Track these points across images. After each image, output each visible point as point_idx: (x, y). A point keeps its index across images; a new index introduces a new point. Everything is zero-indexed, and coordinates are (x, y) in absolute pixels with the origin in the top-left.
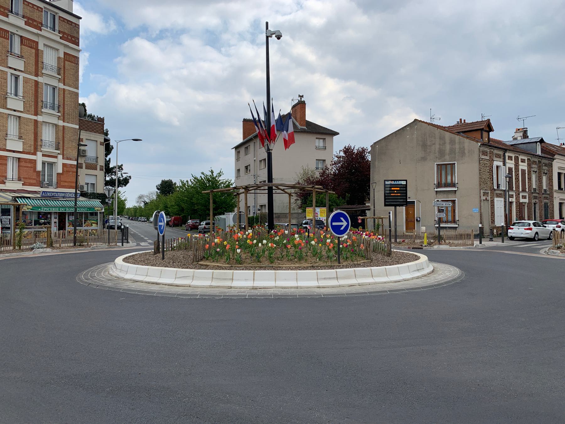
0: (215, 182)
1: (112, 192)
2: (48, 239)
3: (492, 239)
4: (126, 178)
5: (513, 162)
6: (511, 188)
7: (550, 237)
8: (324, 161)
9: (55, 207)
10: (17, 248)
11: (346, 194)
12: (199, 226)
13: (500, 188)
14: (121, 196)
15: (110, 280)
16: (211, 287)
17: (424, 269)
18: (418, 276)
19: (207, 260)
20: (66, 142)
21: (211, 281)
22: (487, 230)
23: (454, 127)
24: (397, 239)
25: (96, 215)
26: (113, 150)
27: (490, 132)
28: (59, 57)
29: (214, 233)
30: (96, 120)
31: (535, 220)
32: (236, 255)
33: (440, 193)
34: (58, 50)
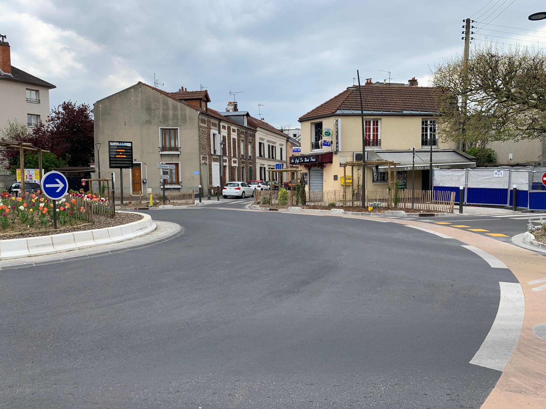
3: (210, 198)
5: (226, 131)
6: (224, 153)
7: (253, 195)
8: (38, 116)
11: (66, 155)
13: (216, 153)
17: (147, 228)
18: (141, 235)
22: (206, 190)
23: (176, 94)
24: (124, 201)
27: (208, 103)
31: (243, 181)
33: (164, 156)
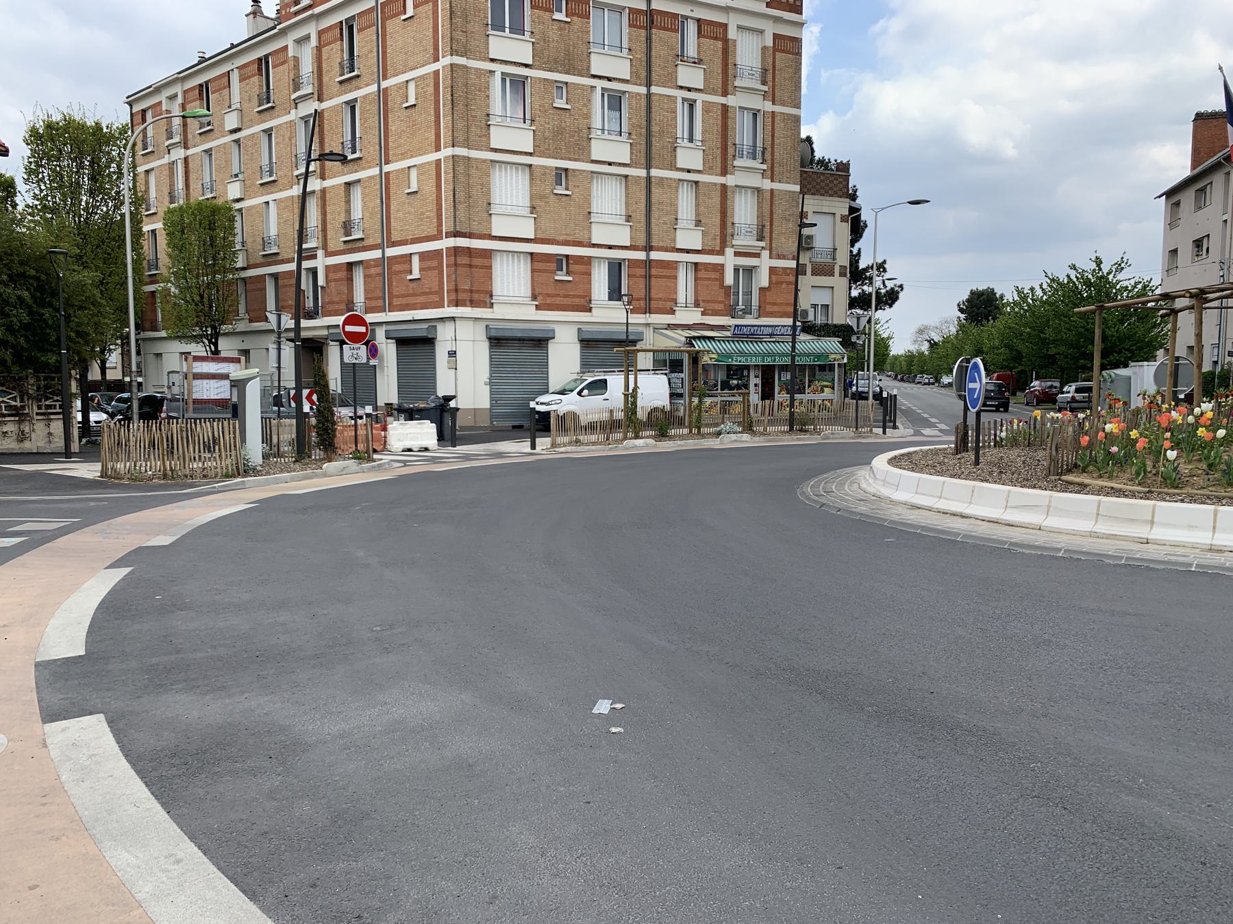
0: (1105, 287)
1: (864, 321)
2: (744, 417)
4: (892, 289)
9: (755, 355)
10: (695, 431)
12: (1060, 396)
14: (881, 329)
15: (863, 500)
16: (1093, 534)
19: (1084, 471)
20: (775, 223)
21: (1094, 522)
25: (830, 370)
26: (867, 230)
28: (765, 47)
29: (1101, 410)
30: (832, 170)
32: (1164, 465)
34: (761, 32)
